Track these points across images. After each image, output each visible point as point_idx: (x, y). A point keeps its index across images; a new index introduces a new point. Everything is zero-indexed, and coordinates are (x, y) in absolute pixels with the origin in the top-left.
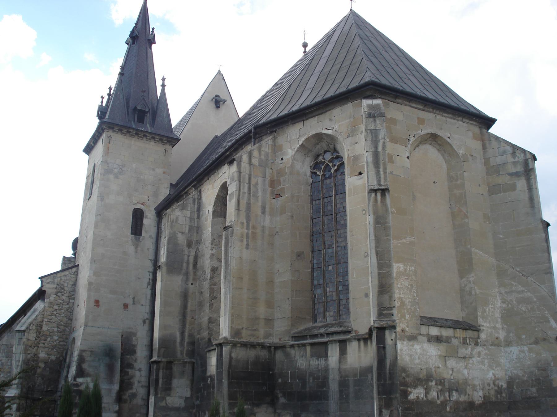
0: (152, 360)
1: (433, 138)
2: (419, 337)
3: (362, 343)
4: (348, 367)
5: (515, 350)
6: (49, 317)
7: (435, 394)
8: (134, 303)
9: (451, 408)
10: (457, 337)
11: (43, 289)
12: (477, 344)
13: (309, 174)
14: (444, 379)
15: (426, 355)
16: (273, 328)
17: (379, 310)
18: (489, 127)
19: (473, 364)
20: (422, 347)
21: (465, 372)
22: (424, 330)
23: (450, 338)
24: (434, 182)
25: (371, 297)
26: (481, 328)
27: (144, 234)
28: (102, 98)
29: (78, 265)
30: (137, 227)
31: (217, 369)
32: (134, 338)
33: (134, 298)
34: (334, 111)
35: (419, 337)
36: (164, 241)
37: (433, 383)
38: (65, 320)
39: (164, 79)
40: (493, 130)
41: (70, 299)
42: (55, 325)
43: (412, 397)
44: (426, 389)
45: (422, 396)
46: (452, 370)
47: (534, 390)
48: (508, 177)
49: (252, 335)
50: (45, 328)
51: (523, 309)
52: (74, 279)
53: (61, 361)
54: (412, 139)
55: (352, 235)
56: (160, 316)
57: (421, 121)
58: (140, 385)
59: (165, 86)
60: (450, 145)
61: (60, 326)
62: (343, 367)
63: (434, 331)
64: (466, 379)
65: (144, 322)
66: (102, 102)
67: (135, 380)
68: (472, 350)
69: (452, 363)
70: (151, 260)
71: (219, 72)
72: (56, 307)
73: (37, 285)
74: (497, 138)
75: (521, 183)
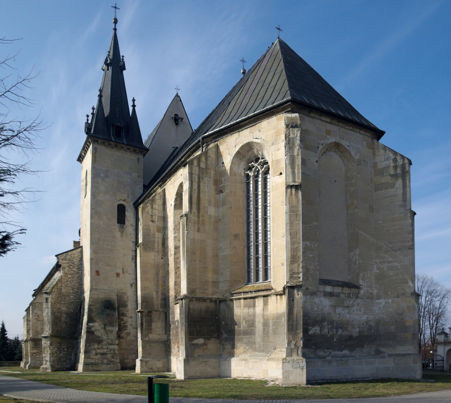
0: (138, 310)
1: (337, 145)
2: (318, 293)
3: (294, 190)
4: (269, 313)
5: (382, 301)
6: (66, 283)
7: (326, 330)
8: (123, 273)
9: (337, 340)
10: (344, 293)
11: (59, 264)
12: (357, 297)
13: (243, 175)
14: (333, 321)
15: (322, 305)
16: (218, 288)
17: (290, 274)
18: (379, 138)
19: (353, 311)
20: (320, 300)
21: (348, 316)
22: (322, 288)
23: (339, 293)
24: (335, 181)
25: (285, 265)
26: (361, 287)
27: (126, 222)
28: (273, 44)
29: (82, 247)
30: (121, 220)
31: (180, 316)
32: (126, 296)
33: (123, 269)
34: (262, 123)
35: (318, 293)
36: (140, 227)
37: (326, 323)
38: (77, 285)
39: (134, 100)
40: (383, 141)
41: (79, 270)
42: (70, 288)
43: (311, 332)
44: (321, 327)
45: (318, 332)
46: (339, 314)
47: (393, 328)
48: (390, 178)
49: (204, 293)
50: (63, 290)
51: (391, 274)
52: (80, 257)
53: (77, 312)
54: (321, 147)
55: (274, 221)
56: (141, 281)
57: (328, 132)
58: (132, 327)
59: (135, 106)
60: (348, 150)
61: (74, 289)
62: (266, 313)
63: (329, 289)
64: (348, 321)
65: (132, 285)
66: (88, 120)
67: (128, 324)
68: (354, 301)
69: (339, 310)
70: (133, 242)
71: (177, 96)
72: (70, 276)
73: (54, 261)
74: (385, 148)
75: (399, 182)
